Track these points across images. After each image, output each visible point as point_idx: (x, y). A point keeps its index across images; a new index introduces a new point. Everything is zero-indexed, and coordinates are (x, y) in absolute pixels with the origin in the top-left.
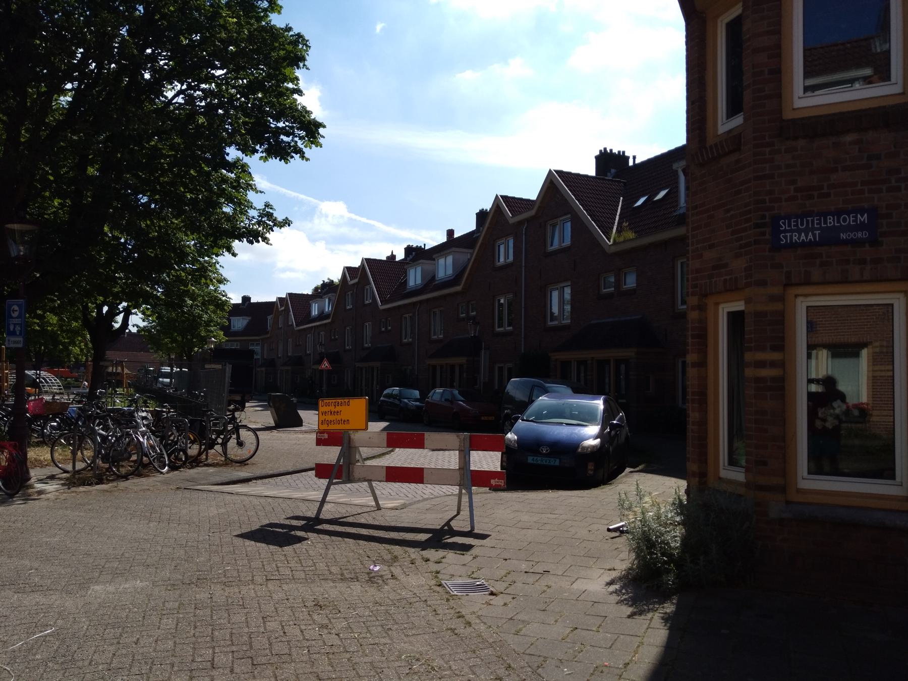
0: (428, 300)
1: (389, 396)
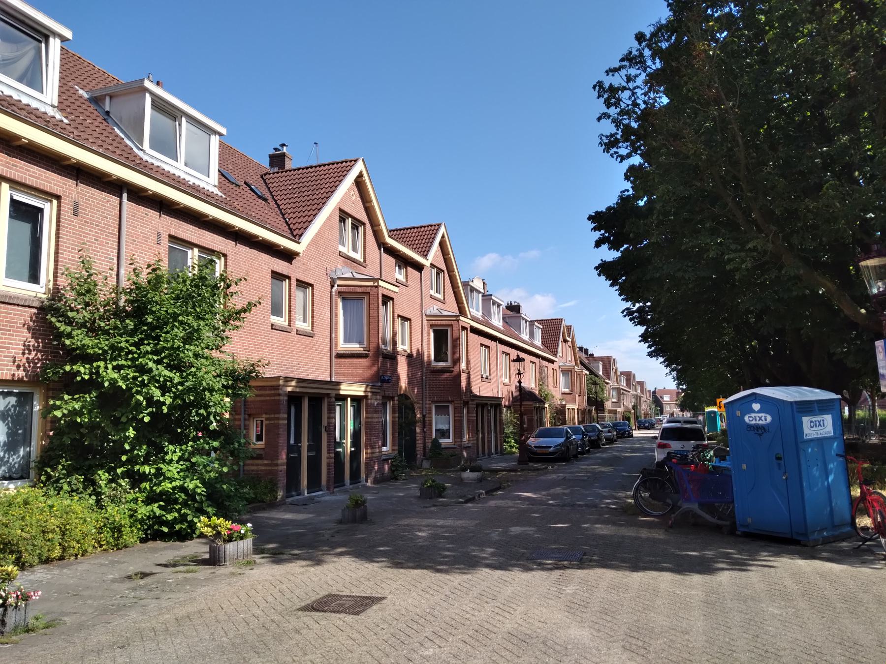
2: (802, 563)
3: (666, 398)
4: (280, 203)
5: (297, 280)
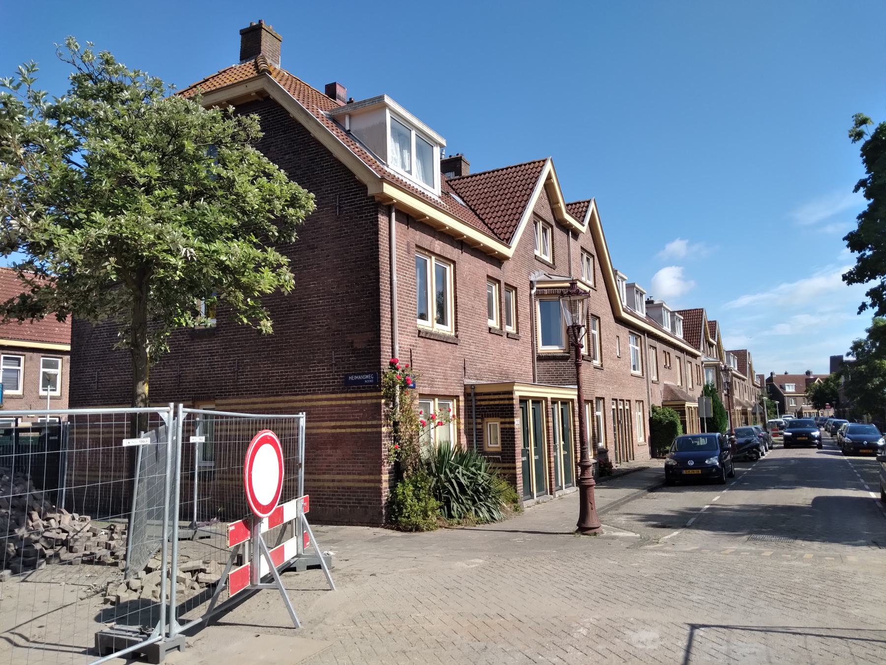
3: (790, 388)
4: (456, 188)
5: (506, 284)
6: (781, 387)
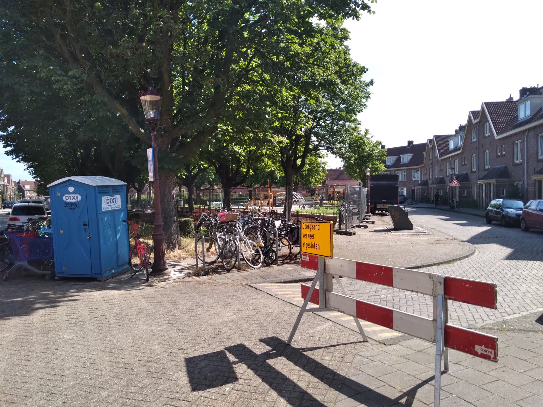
0: (535, 127)
1: (495, 206)
2: (96, 295)
3: (27, 187)
6: (23, 186)
